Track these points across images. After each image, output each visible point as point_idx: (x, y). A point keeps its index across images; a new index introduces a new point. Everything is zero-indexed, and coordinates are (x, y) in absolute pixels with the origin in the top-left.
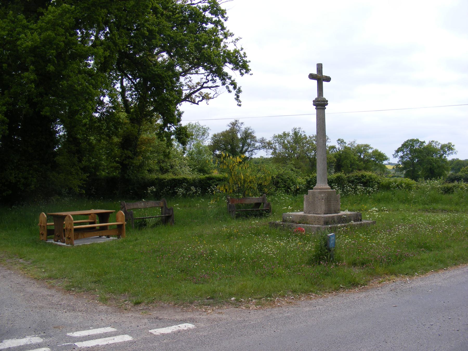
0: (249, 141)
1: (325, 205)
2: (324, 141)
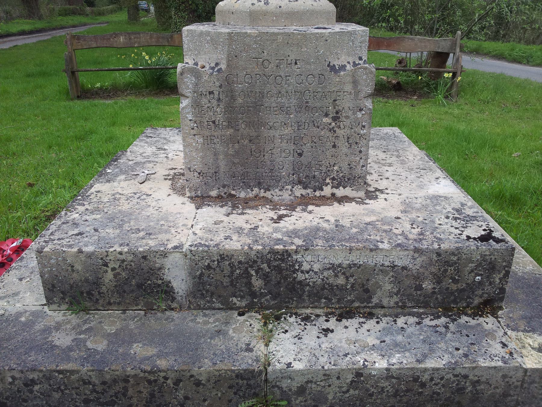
1: (209, 140)
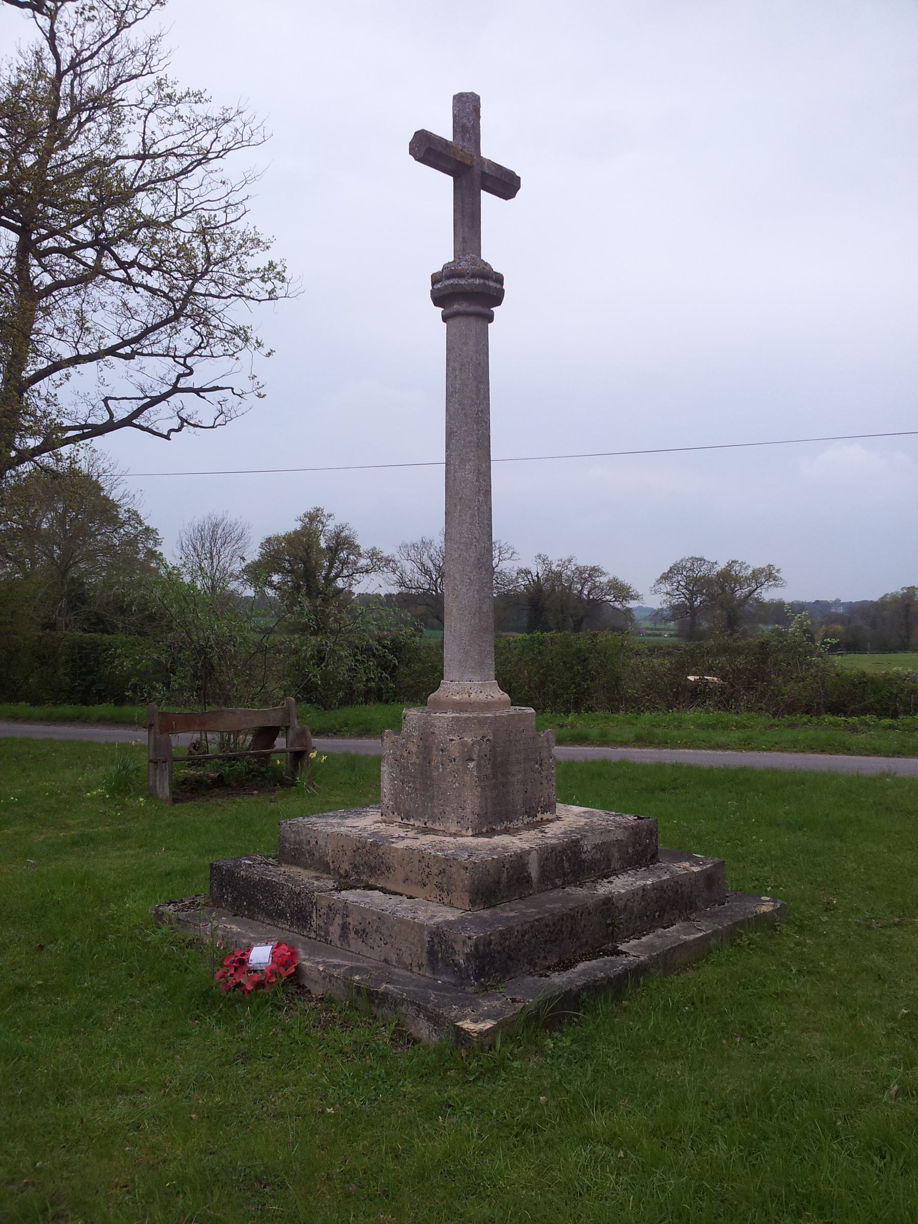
0: (343, 555)
2: (479, 473)
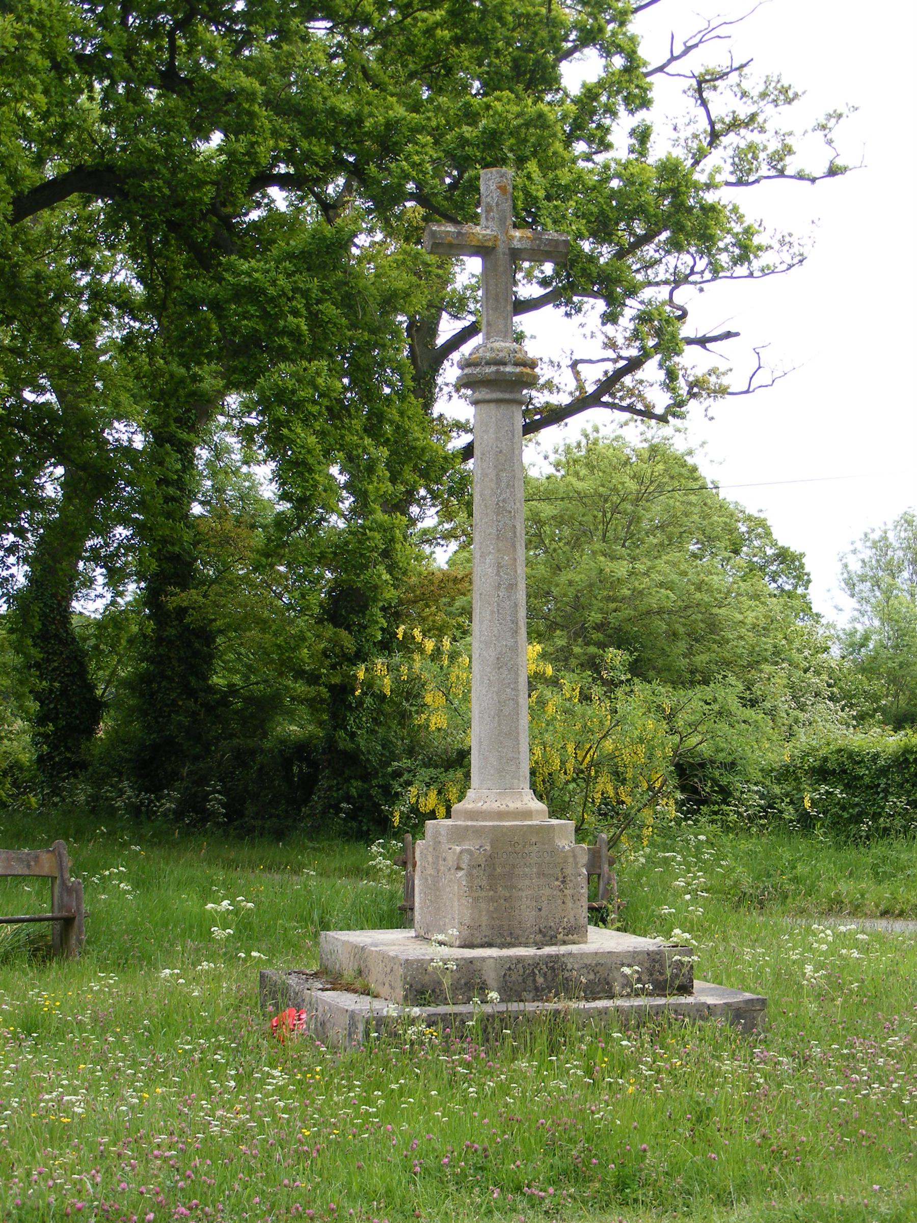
1: (476, 900)
